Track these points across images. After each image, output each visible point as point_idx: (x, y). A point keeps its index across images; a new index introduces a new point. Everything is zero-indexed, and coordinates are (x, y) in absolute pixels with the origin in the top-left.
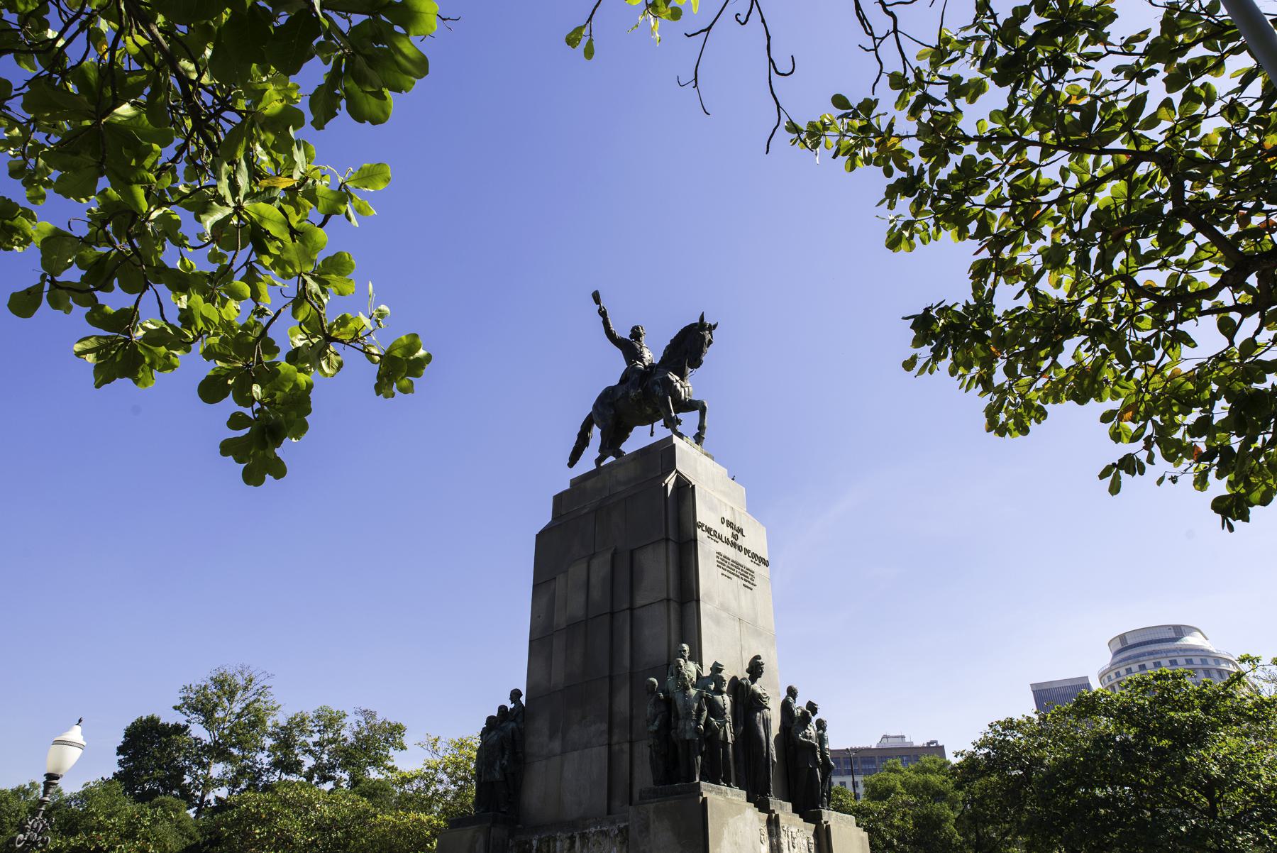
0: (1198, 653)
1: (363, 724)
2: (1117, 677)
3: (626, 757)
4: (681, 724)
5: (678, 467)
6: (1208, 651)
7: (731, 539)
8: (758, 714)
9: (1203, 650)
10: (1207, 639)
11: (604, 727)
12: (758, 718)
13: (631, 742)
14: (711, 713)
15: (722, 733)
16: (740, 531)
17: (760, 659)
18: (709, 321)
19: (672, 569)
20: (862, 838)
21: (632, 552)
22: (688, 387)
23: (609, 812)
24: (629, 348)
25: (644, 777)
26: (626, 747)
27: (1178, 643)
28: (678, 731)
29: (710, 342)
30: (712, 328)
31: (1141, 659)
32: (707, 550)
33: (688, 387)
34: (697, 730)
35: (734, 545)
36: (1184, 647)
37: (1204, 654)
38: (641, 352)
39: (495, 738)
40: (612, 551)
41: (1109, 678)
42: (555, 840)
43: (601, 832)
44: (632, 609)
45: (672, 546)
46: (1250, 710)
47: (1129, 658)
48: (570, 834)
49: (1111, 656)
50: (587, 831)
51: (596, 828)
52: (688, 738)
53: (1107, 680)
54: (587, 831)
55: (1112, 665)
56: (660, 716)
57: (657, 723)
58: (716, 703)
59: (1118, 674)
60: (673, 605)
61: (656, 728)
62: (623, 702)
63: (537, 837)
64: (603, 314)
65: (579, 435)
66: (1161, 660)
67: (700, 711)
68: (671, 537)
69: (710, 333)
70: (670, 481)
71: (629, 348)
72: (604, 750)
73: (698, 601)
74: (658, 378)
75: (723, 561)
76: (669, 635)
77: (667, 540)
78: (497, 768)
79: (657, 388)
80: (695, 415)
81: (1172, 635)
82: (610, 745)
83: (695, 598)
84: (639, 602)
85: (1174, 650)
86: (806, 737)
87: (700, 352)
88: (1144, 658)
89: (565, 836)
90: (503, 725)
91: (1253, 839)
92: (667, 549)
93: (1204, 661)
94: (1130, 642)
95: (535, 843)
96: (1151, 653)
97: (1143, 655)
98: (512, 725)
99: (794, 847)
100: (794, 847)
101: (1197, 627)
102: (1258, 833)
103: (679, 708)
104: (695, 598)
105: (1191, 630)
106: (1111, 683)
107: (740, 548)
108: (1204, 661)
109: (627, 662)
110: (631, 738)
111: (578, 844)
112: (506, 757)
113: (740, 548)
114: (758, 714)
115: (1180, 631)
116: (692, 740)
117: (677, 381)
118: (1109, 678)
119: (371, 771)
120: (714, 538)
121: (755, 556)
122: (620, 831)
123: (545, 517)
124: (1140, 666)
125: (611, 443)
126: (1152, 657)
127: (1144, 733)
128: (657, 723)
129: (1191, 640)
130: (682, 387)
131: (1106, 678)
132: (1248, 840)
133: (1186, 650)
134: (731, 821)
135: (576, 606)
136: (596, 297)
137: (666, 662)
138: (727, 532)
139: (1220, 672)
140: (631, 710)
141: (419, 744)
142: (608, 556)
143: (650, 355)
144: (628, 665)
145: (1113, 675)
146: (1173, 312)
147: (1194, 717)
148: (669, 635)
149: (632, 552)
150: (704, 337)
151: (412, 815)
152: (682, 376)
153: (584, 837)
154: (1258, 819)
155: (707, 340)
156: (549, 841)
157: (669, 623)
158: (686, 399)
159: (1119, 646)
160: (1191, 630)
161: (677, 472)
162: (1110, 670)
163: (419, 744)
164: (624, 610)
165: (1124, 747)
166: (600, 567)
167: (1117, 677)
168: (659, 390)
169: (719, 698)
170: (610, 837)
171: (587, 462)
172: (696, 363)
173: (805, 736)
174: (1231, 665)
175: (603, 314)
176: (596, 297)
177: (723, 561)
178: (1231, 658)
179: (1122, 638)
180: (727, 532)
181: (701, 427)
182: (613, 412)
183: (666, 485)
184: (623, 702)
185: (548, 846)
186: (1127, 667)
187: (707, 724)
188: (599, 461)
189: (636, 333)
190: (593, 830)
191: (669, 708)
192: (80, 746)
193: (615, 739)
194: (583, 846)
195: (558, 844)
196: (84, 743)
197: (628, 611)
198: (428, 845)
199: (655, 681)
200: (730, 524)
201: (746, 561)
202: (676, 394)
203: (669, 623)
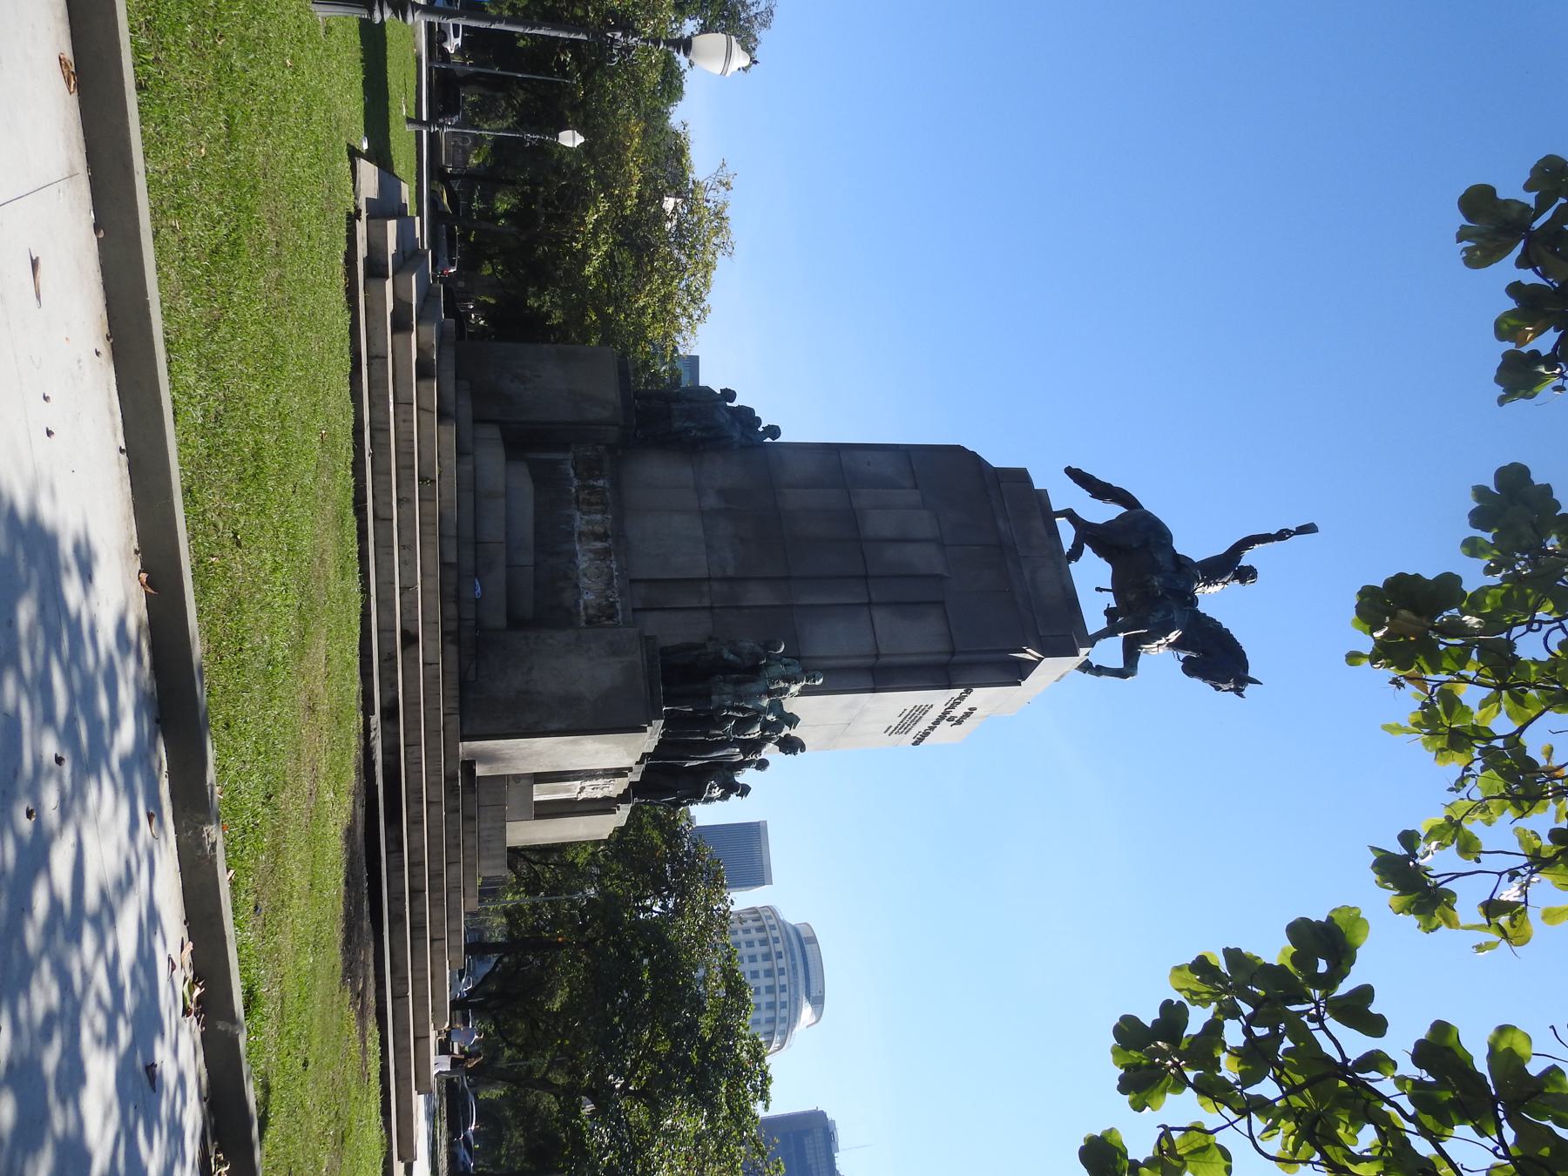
0: (792, 1016)
1: (754, 10)
2: (770, 926)
3: (695, 603)
4: (729, 688)
5: (1047, 660)
6: (794, 1027)
7: (948, 716)
8: (738, 750)
9: (795, 1021)
10: (807, 1027)
11: (730, 572)
12: (733, 750)
13: (711, 608)
14: (739, 720)
15: (717, 732)
16: (959, 722)
17: (801, 751)
18: (1249, 689)
19: (914, 659)
20: (602, 835)
21: (941, 603)
22: (1160, 657)
23: (632, 581)
24: (1228, 566)
25: (675, 630)
26: (706, 602)
27: (804, 998)
28: (722, 684)
29: (1218, 689)
30: (1239, 692)
31: (789, 956)
32: (938, 699)
33: (1160, 657)
34: (721, 708)
35: (942, 717)
36: (799, 1003)
37: (791, 1021)
38: (1216, 584)
39: (722, 420)
40: (946, 574)
41: (770, 917)
42: (604, 512)
43: (612, 578)
44: (870, 604)
45: (945, 658)
46: (728, 1149)
47: (790, 943)
48: (609, 533)
49: (793, 924)
50: (613, 557)
51: (616, 570)
52: (713, 697)
53: (766, 914)
54: (613, 557)
55: (784, 923)
56: (738, 660)
57: (732, 657)
58: (752, 726)
59: (776, 940)
60: (870, 661)
61: (726, 656)
62: (759, 596)
63: (607, 486)
64: (1282, 535)
65: (1108, 486)
66: (784, 960)
67: (744, 710)
68: (955, 658)
69: (1230, 690)
70: (1031, 654)
71: (1228, 566)
72: (702, 572)
73: (874, 690)
74: (1176, 616)
75: (923, 710)
76: (837, 657)
77: (953, 653)
78: (686, 425)
79: (1159, 615)
80: (1119, 664)
81: (813, 994)
82: (709, 579)
83: (878, 687)
84: (880, 616)
85: (796, 991)
86: (711, 788)
87: (1205, 676)
88: (789, 960)
89: (608, 526)
90: (737, 424)
91: (603, 1142)
92: (940, 653)
93: (783, 1020)
94: (808, 947)
95: (601, 483)
96: (794, 967)
97: (793, 959)
98: (737, 435)
99: (593, 789)
100: (593, 789)
101: (820, 1022)
102: (609, 1147)
103: (748, 686)
104: (878, 687)
105: (819, 1014)
106: (764, 918)
107: (937, 722)
108: (783, 1020)
109: (806, 600)
110: (716, 608)
111: (599, 545)
112: (699, 434)
113: (937, 722)
114: (738, 750)
115: (818, 1002)
116: (710, 702)
117: (1167, 640)
118: (770, 917)
119: (694, 22)
120: (952, 702)
121: (926, 734)
122: (612, 605)
123: (998, 457)
124: (781, 953)
125: (1089, 534)
126: (790, 967)
127: (705, 1047)
128: (732, 657)
129: (807, 1012)
130: (1159, 645)
131: (769, 913)
132: (602, 1137)
133: (796, 1004)
134: (621, 749)
135: (879, 524)
136: (1308, 529)
137: (802, 655)
138: (958, 712)
139: (771, 1033)
140: (748, 607)
141: (724, 165)
142: (939, 570)
143: (1213, 599)
144: (800, 603)
145: (772, 922)
146: (1192, 1081)
147: (721, 1109)
148: (837, 657)
149: (941, 603)
150: (1226, 682)
151: (637, 175)
152: (1174, 646)
153: (606, 553)
154: (621, 1148)
155: (1221, 685)
156: (602, 504)
157: (847, 657)
158: (1142, 649)
159: (804, 935)
160: (819, 1014)
161: (1041, 659)
162: (778, 920)
163: (724, 165)
164: (869, 594)
165: (692, 1027)
166: (925, 558)
167: (770, 926)
168: (1157, 617)
169: (757, 728)
170: (605, 589)
171: (1064, 495)
172: (1190, 668)
173: (712, 787)
174: (778, 1045)
175: (1282, 535)
176: (1308, 529)
177: (923, 710)
178: (786, 1045)
179: (813, 940)
180: (958, 712)
181: (1099, 671)
182: (1135, 546)
183: (1025, 652)
184: (759, 596)
185: (597, 504)
186: (783, 953)
187: (728, 718)
188: (1070, 515)
189: (1246, 575)
190: (614, 566)
191: (750, 671)
192: (723, 73)
193: (716, 586)
194: (595, 552)
195: (599, 517)
196: (728, 74)
197: (866, 601)
198: (602, 195)
199: (781, 650)
200: (967, 715)
201: (922, 726)
202: (1150, 638)
203: (847, 657)
